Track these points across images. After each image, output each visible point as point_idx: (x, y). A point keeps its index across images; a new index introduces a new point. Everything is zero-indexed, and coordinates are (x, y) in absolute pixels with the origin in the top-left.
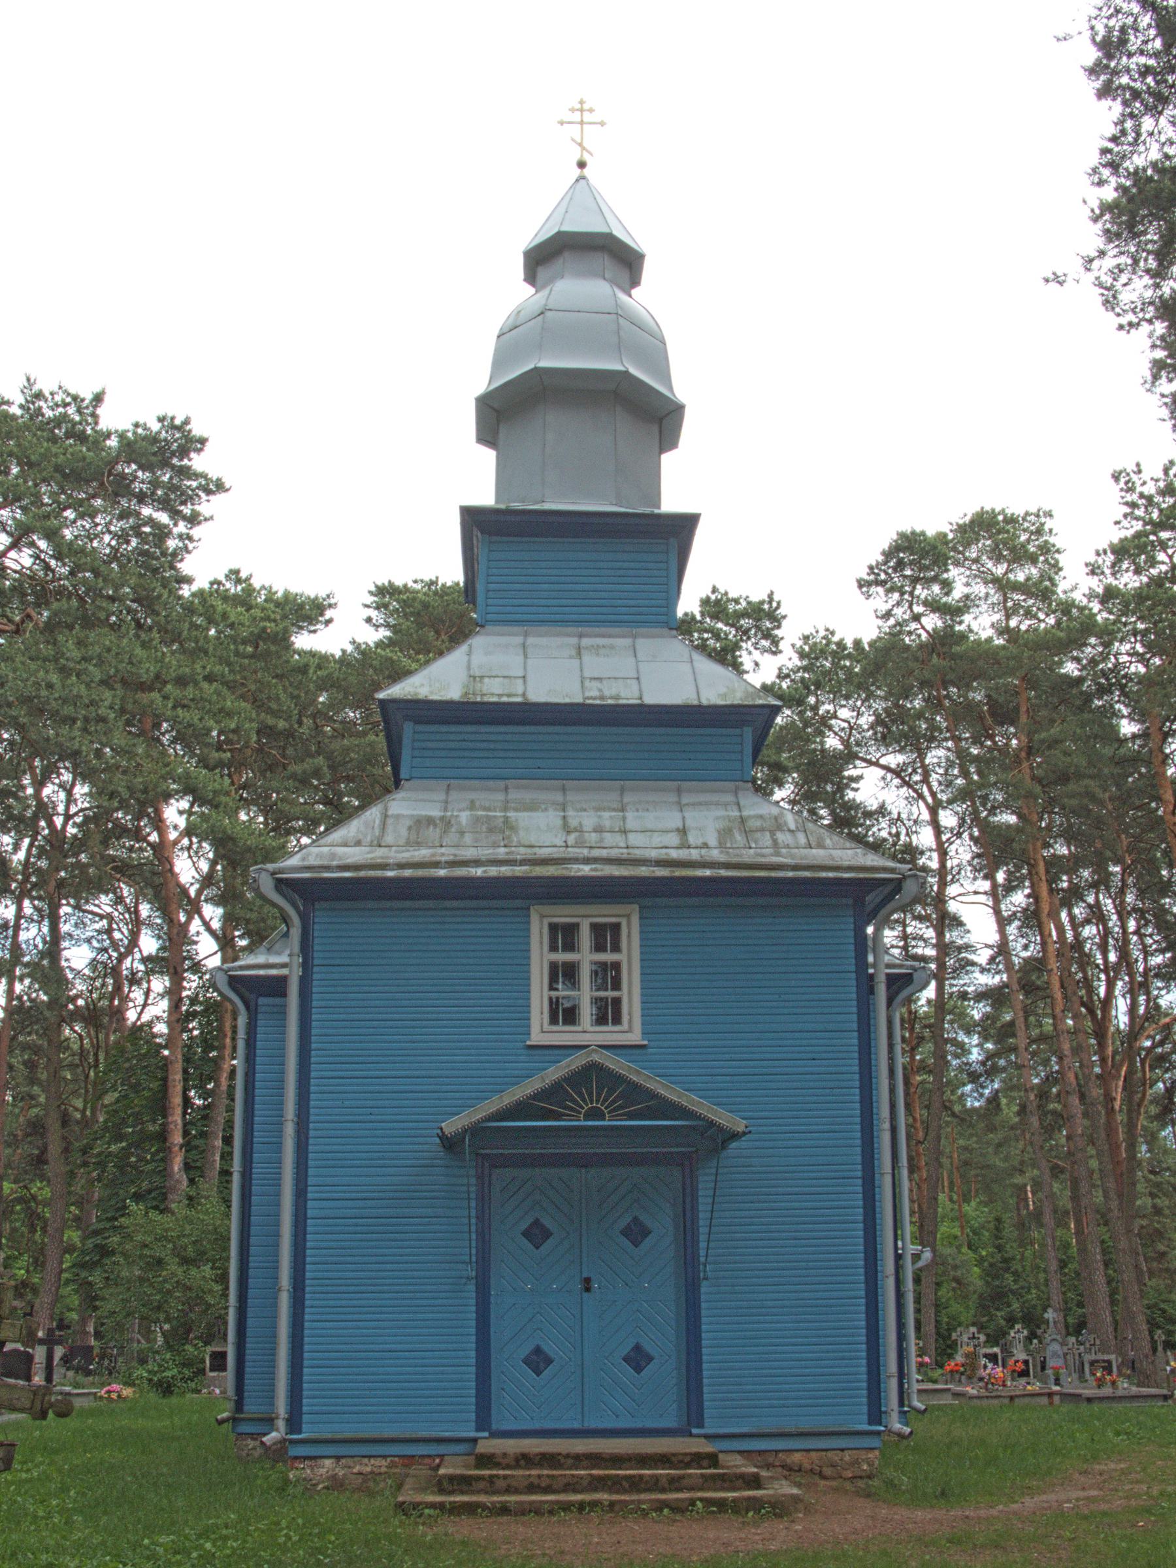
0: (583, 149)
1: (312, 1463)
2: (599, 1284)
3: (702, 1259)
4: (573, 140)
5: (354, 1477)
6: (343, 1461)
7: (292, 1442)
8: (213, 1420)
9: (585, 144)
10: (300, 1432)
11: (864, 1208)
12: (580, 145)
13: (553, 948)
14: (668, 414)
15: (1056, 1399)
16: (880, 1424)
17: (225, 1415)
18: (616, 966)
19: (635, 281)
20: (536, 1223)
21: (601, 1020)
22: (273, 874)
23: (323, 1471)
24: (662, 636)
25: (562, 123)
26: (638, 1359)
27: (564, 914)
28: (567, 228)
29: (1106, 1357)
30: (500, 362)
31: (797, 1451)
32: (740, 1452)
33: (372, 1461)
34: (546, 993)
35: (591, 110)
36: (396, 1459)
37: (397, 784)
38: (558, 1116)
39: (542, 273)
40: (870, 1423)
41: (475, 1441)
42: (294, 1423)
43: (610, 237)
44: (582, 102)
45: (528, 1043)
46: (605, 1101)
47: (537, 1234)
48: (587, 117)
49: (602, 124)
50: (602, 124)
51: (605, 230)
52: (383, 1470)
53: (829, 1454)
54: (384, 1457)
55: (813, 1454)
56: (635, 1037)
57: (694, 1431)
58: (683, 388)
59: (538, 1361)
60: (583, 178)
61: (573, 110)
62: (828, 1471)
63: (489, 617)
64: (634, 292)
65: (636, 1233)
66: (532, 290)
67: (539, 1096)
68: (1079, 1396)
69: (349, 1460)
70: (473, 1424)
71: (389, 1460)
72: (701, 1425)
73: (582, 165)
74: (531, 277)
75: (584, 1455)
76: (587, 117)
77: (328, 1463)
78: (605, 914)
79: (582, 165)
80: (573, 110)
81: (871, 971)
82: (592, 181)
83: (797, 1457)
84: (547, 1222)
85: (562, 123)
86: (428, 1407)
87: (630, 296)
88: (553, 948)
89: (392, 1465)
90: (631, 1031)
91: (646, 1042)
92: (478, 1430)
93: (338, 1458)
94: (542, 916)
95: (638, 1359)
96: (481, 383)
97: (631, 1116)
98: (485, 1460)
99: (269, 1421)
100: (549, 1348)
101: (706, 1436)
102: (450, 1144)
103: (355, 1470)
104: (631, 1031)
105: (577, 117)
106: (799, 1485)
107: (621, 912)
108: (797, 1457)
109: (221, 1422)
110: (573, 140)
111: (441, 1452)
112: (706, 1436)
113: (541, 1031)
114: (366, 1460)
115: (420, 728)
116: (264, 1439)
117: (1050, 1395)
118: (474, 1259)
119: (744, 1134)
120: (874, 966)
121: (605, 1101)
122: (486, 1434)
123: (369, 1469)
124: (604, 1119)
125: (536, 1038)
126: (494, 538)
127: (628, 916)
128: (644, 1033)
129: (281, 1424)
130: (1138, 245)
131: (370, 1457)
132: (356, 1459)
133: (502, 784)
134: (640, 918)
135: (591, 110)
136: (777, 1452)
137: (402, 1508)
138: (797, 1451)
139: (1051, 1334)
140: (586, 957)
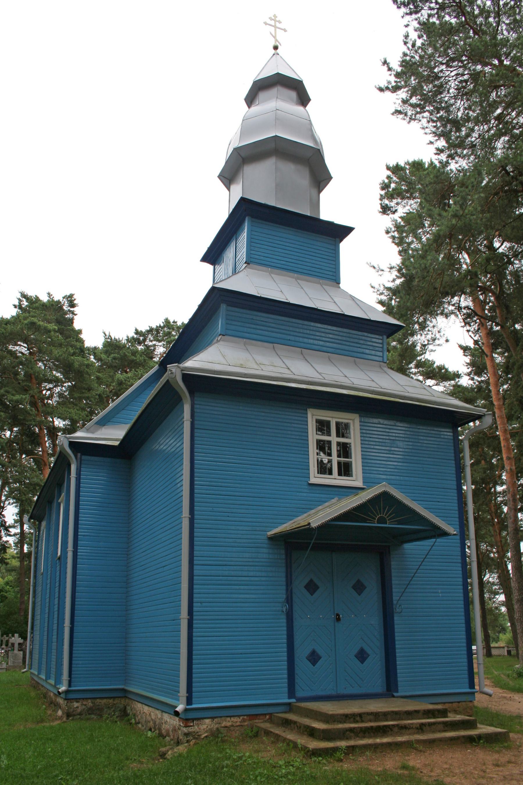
0: (276, 41)
1: (199, 722)
2: (343, 615)
5: (222, 729)
6: (216, 720)
9: (278, 38)
12: (275, 37)
14: (324, 180)
20: (311, 581)
22: (68, 438)
23: (205, 726)
24: (333, 286)
25: (266, 24)
26: (362, 656)
30: (244, 131)
33: (232, 719)
34: (316, 457)
35: (280, 22)
36: (245, 717)
38: (365, 521)
44: (275, 16)
48: (278, 25)
49: (285, 30)
52: (238, 724)
54: (239, 716)
56: (359, 484)
57: (395, 694)
61: (271, 19)
63: (252, 260)
65: (359, 588)
67: (356, 509)
69: (219, 719)
70: (287, 695)
71: (241, 718)
73: (276, 48)
75: (351, 714)
77: (207, 721)
78: (344, 417)
79: (276, 48)
80: (271, 19)
84: (316, 581)
89: (244, 720)
92: (289, 698)
93: (213, 718)
94: (313, 415)
103: (223, 725)
105: (272, 23)
107: (350, 418)
114: (229, 719)
123: (230, 724)
124: (386, 523)
125: (313, 480)
126: (254, 219)
127: (353, 420)
131: (230, 717)
132: (223, 718)
140: (334, 439)
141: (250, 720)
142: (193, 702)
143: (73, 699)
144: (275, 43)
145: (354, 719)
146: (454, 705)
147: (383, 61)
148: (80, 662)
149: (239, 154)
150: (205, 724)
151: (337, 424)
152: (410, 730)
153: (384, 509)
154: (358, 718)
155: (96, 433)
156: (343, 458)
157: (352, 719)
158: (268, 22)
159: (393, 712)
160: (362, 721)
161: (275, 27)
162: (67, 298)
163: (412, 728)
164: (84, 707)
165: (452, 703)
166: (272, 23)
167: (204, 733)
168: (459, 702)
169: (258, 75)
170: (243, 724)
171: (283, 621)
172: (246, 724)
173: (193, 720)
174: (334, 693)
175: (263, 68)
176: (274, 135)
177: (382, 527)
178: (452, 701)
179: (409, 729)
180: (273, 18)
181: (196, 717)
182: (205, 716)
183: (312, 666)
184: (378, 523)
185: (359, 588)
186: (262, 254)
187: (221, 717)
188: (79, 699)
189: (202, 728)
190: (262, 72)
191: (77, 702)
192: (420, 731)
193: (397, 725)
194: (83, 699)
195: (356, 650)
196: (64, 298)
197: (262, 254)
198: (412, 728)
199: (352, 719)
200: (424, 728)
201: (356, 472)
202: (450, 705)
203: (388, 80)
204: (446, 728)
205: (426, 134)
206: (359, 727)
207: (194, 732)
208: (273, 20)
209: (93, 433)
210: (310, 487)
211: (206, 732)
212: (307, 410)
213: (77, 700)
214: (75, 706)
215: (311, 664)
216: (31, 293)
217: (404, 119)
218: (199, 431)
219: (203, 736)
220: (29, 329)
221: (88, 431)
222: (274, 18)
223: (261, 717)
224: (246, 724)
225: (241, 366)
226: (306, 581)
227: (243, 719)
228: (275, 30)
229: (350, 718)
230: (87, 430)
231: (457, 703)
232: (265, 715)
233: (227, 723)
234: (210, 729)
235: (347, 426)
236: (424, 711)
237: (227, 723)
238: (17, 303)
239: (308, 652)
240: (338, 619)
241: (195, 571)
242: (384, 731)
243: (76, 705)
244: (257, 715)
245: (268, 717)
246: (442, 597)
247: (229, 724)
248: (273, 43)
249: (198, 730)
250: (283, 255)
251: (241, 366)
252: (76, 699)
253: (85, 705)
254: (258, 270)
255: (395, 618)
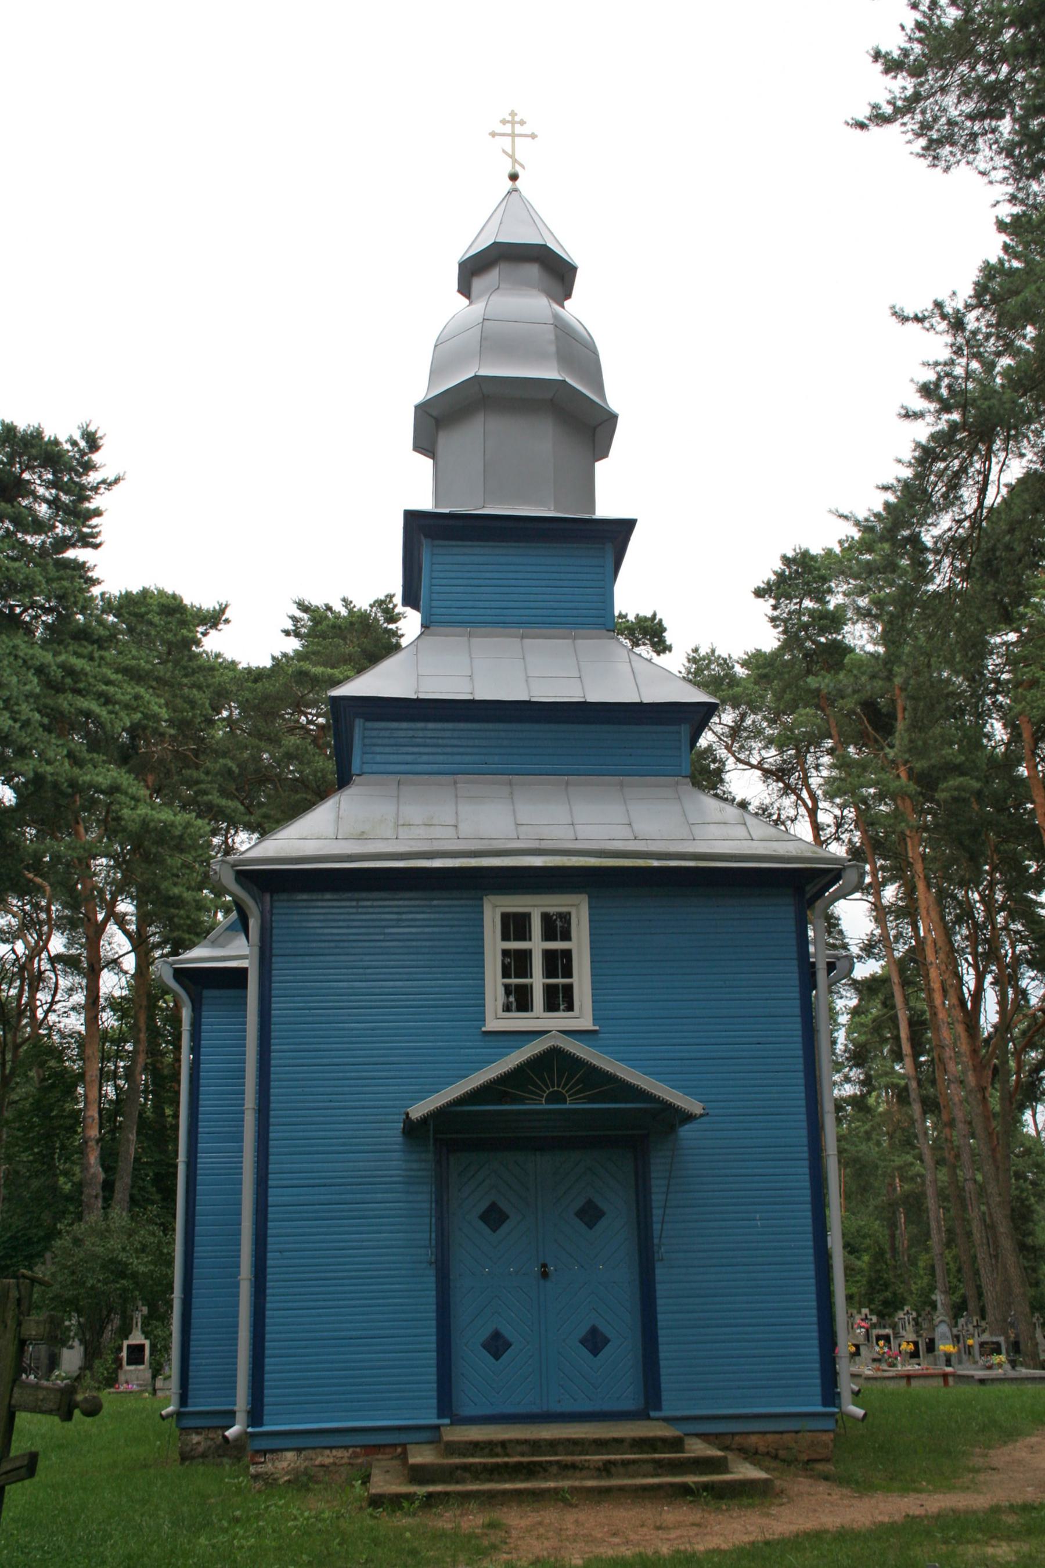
0: (515, 161)
1: (274, 1456)
3: (656, 1241)
4: (504, 152)
6: (304, 1453)
7: (252, 1435)
8: (157, 1415)
9: (517, 157)
10: (261, 1425)
11: (437, 1291)
12: (512, 157)
13: (505, 937)
15: (951, 1380)
16: (834, 1406)
17: (171, 1409)
18: (567, 954)
19: (568, 295)
21: (551, 1006)
22: (171, 964)
23: (285, 1464)
25: (493, 134)
26: (595, 1342)
27: (516, 904)
28: (500, 240)
29: (995, 1339)
30: (436, 371)
31: (753, 1433)
32: (698, 1435)
33: (334, 1452)
35: (522, 123)
36: (358, 1450)
37: (344, 780)
38: (515, 1100)
39: (478, 284)
40: (825, 1405)
41: (437, 1428)
42: (255, 1416)
43: (544, 248)
44: (513, 114)
45: (484, 1029)
46: (566, 1085)
47: (494, 1217)
48: (519, 129)
49: (533, 136)
50: (533, 136)
51: (541, 242)
52: (345, 1460)
53: (785, 1436)
54: (346, 1448)
55: (770, 1437)
57: (652, 1414)
58: (614, 401)
59: (497, 1345)
60: (516, 190)
61: (504, 122)
62: (782, 1453)
63: (434, 618)
64: (567, 303)
65: (590, 1214)
66: (466, 302)
68: (972, 1377)
69: (310, 1451)
71: (351, 1450)
72: (658, 1407)
73: (514, 177)
74: (465, 289)
75: (485, 1442)
76: (519, 129)
77: (290, 1455)
78: (554, 903)
79: (514, 177)
80: (504, 122)
81: (812, 960)
82: (524, 193)
83: (754, 1439)
84: (503, 1205)
85: (493, 134)
86: (411, 1394)
87: (563, 307)
88: (505, 937)
89: (355, 1455)
90: (582, 1017)
91: (597, 1028)
92: (439, 1417)
93: (299, 1450)
95: (595, 1342)
96: (419, 391)
97: (591, 1100)
98: (452, 1449)
99: (230, 1416)
100: (508, 1332)
101: (666, 1419)
102: (413, 1130)
103: (317, 1463)
104: (582, 1017)
105: (507, 128)
106: (767, 1470)
108: (754, 1439)
109: (163, 1418)
110: (504, 152)
111: (403, 1442)
112: (666, 1419)
113: (496, 1020)
114: (328, 1452)
115: (369, 724)
116: (227, 1433)
117: (945, 1376)
118: (433, 1242)
119: (702, 1115)
120: (815, 955)
121: (566, 1085)
122: (447, 1421)
123: (331, 1460)
124: (565, 1103)
125: (492, 1024)
126: (437, 542)
128: (596, 1020)
129: (241, 1417)
130: (961, 345)
131: (331, 1448)
132: (318, 1451)
133: (450, 778)
134: (590, 908)
135: (522, 123)
136: (733, 1434)
137: (376, 1501)
138: (753, 1433)
139: (941, 1315)
140: (537, 945)
141: (367, 1454)
142: (265, 1422)
143: (190, 1428)
144: (513, 167)
145: (492, 1450)
146: (786, 1437)
147: (872, 53)
148: (204, 1361)
149: (426, 412)
150: (285, 1460)
151: (546, 918)
152: (584, 1472)
153: (560, 1078)
154: (499, 1450)
155: (229, 946)
156: (563, 977)
157: (487, 1451)
158: (497, 131)
159: (568, 1440)
160: (507, 1455)
161: (513, 135)
162: (380, 605)
163: (588, 1468)
164: (209, 1443)
165: (782, 1433)
166: (507, 128)
167: (284, 1475)
168: (797, 1432)
169: (471, 246)
170: (352, 1461)
171: (430, 1281)
172: (360, 1461)
173: (265, 1452)
174: (535, 1409)
175: (482, 229)
176: (472, 375)
177: (560, 1111)
178: (781, 1429)
179: (581, 1469)
180: (509, 118)
181: (269, 1447)
182: (286, 1447)
183: (494, 1361)
184: (548, 1102)
185: (590, 1214)
186: (454, 604)
187: (314, 1448)
188: (202, 1428)
189: (280, 1467)
190: (479, 240)
191: (198, 1433)
192: (604, 1474)
193: (558, 1462)
194: (209, 1428)
195: (583, 1331)
196: (371, 606)
197: (454, 604)
198: (588, 1468)
199: (487, 1451)
200: (613, 1470)
201: (581, 1001)
202: (777, 1436)
203: (872, 102)
204: (660, 1471)
205: (991, 182)
206: (480, 1463)
207: (266, 1473)
208: (508, 122)
209: (223, 946)
210: (487, 1038)
211: (287, 1473)
212: (481, 899)
213: (197, 1430)
214: (194, 1442)
215: (492, 1358)
216: (317, 600)
217: (935, 166)
218: (279, 959)
219: (281, 1481)
220: (299, 683)
221: (214, 944)
222: (512, 120)
223: (388, 1450)
224: (360, 1461)
225: (361, 837)
226: (484, 1205)
227: (354, 1452)
228: (513, 142)
229: (482, 1449)
230: (213, 942)
231: (793, 1435)
232: (394, 1446)
233: (326, 1458)
234: (293, 1469)
235: (566, 918)
236: (634, 1440)
237: (326, 1458)
238: (289, 625)
239: (485, 1333)
240: (545, 1275)
241: (270, 1199)
242: (530, 1471)
243: (195, 1438)
244: (385, 1446)
245: (399, 1450)
246: (763, 1227)
247: (327, 1461)
248: (508, 169)
249: (273, 1470)
250: (497, 597)
251: (361, 837)
252: (197, 1428)
253: (212, 1439)
254: (446, 636)
255: (658, 1271)
